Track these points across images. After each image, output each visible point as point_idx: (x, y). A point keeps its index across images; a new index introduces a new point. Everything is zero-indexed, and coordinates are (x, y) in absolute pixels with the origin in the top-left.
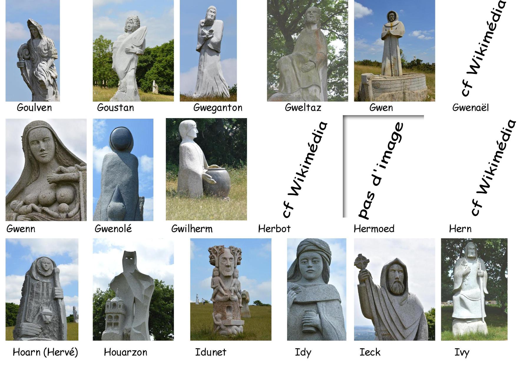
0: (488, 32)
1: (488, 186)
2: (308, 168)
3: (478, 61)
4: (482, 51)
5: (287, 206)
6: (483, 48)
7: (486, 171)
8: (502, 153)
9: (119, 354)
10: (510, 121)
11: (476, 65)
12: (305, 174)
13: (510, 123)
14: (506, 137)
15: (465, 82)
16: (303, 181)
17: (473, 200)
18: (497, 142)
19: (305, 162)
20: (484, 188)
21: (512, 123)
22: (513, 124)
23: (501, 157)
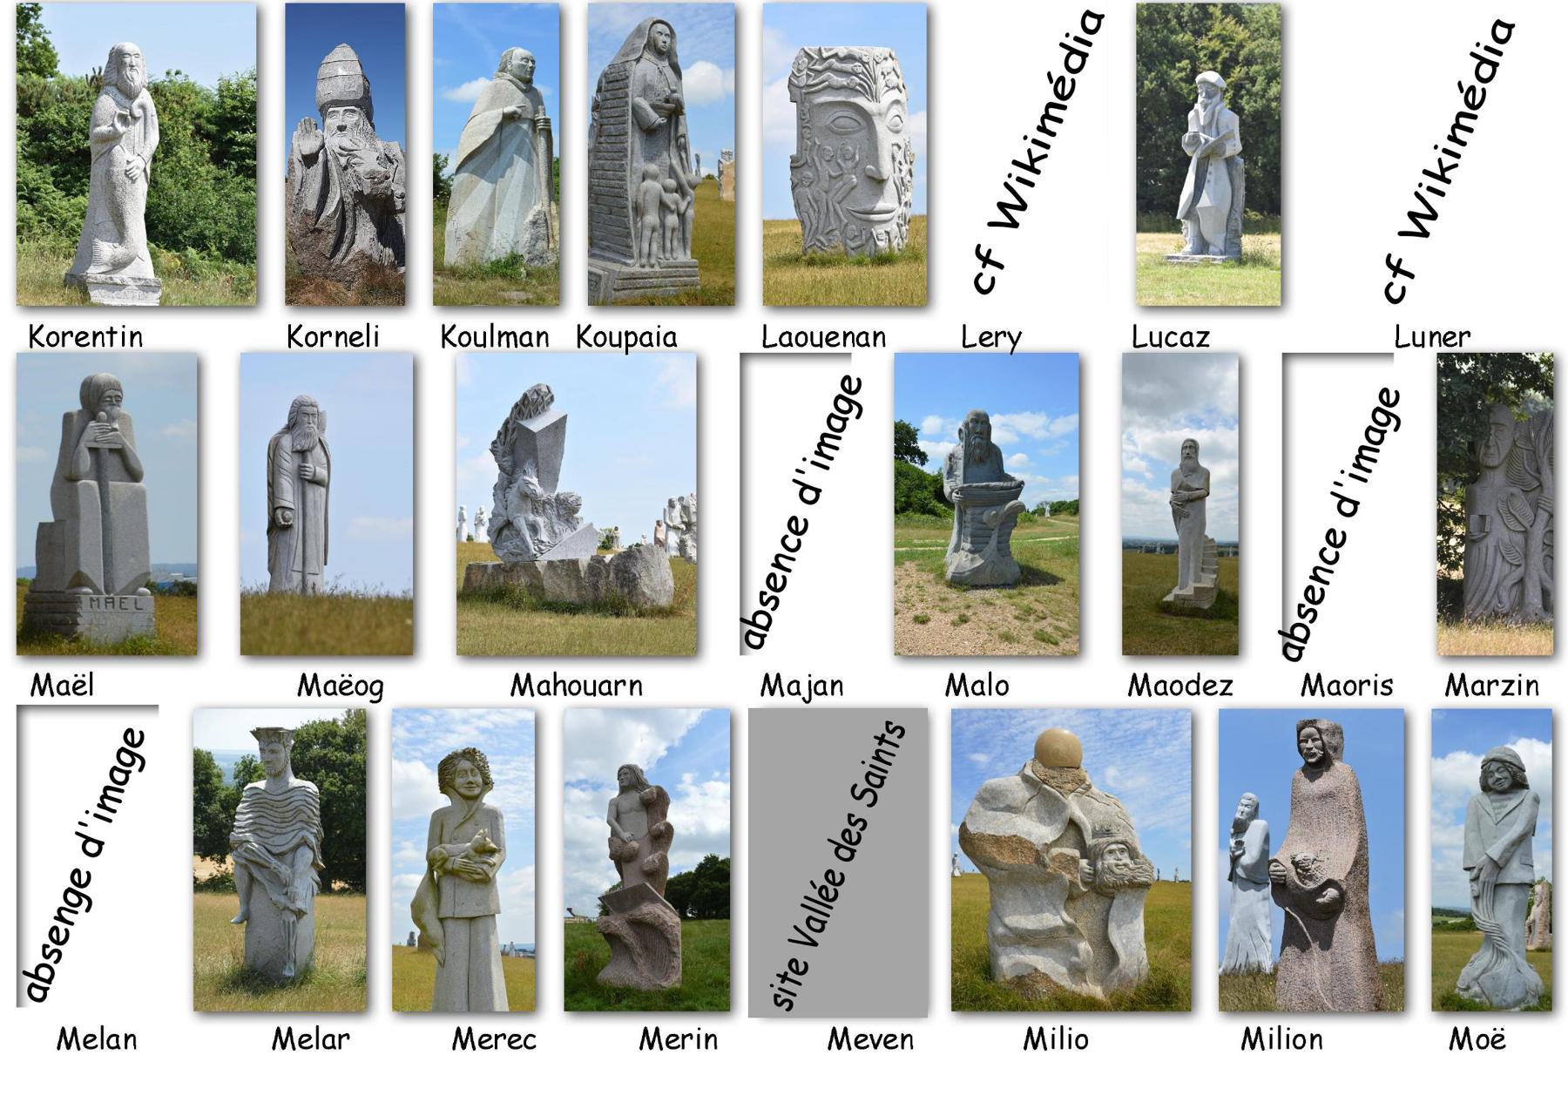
1: (1023, 207)
3: (1431, 198)
4: (1033, 161)
5: (986, 260)
7: (1426, 172)
8: (1475, 117)
9: (590, 690)
12: (1448, 175)
13: (1499, 28)
14: (1486, 71)
16: (1442, 194)
17: (1389, 256)
18: (1049, 75)
19: (1039, 129)
20: (1420, 222)
21: (1503, 30)
23: (1060, 121)
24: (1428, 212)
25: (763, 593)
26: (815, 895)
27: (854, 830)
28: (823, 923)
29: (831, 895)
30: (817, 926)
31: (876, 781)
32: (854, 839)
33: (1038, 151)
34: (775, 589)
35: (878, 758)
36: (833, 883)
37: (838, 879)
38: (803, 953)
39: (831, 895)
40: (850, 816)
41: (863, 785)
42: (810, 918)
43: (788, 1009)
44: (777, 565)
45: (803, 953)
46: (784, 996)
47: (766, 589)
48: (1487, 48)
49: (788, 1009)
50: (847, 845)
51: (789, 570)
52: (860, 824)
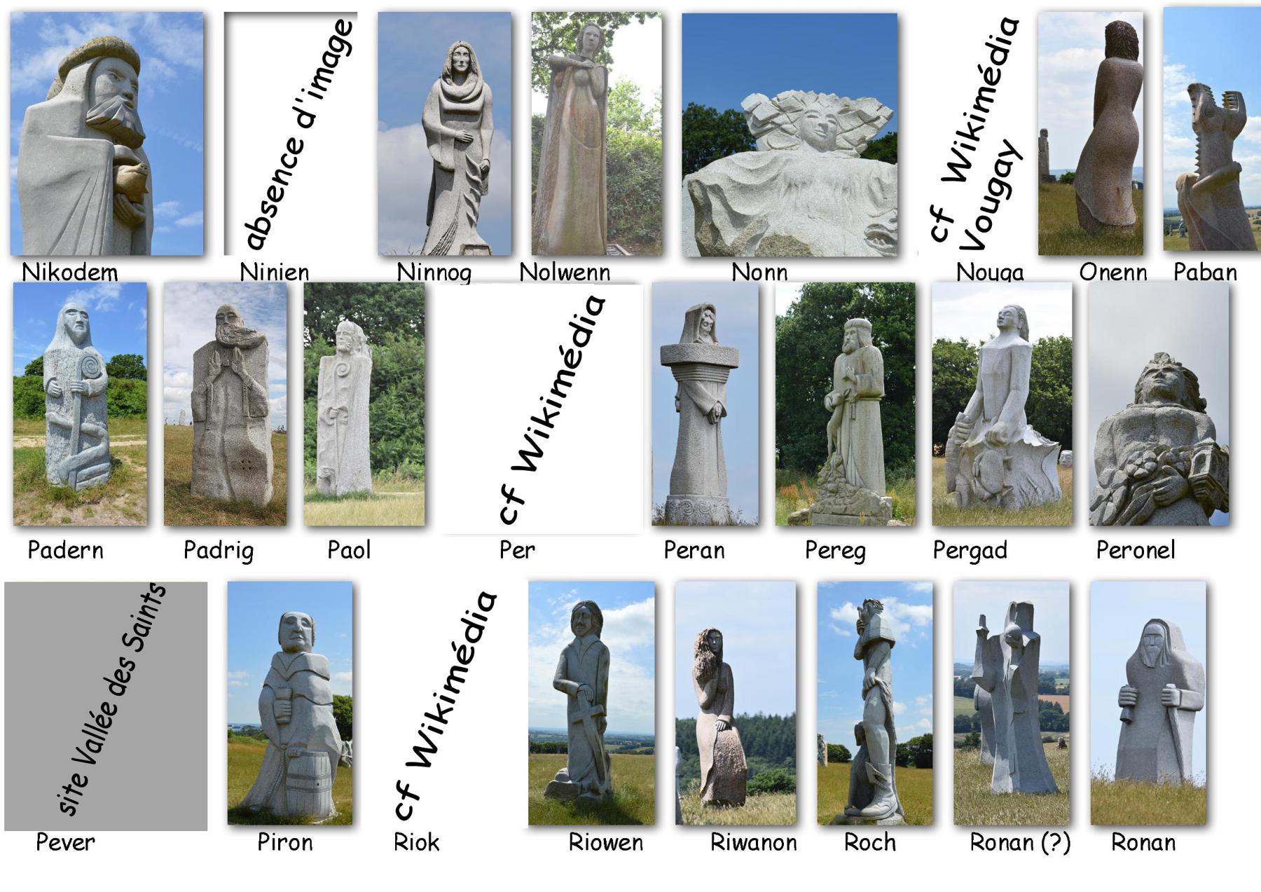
0: (562, 372)
2: (453, 702)
3: (538, 439)
6: (551, 409)
10: (484, 594)
11: (534, 451)
13: (484, 599)
15: (508, 491)
18: (561, 348)
19: (975, 107)
20: (529, 459)
22: (489, 601)
23: (569, 385)
24: (535, 451)
25: (264, 203)
26: (93, 722)
27: (125, 670)
28: (100, 745)
29: (106, 723)
30: (95, 747)
31: (143, 631)
32: (125, 677)
33: (445, 705)
34: (274, 199)
35: (144, 613)
36: (108, 713)
37: (112, 710)
38: (83, 770)
39: (106, 723)
40: (122, 659)
41: (132, 634)
42: (89, 741)
43: (72, 815)
44: (277, 179)
45: (83, 770)
46: (69, 804)
47: (267, 199)
48: (475, 615)
49: (72, 815)
50: (119, 682)
51: (286, 184)
52: (130, 666)
